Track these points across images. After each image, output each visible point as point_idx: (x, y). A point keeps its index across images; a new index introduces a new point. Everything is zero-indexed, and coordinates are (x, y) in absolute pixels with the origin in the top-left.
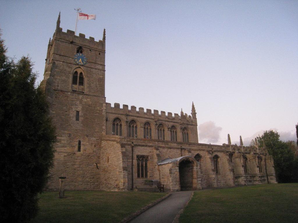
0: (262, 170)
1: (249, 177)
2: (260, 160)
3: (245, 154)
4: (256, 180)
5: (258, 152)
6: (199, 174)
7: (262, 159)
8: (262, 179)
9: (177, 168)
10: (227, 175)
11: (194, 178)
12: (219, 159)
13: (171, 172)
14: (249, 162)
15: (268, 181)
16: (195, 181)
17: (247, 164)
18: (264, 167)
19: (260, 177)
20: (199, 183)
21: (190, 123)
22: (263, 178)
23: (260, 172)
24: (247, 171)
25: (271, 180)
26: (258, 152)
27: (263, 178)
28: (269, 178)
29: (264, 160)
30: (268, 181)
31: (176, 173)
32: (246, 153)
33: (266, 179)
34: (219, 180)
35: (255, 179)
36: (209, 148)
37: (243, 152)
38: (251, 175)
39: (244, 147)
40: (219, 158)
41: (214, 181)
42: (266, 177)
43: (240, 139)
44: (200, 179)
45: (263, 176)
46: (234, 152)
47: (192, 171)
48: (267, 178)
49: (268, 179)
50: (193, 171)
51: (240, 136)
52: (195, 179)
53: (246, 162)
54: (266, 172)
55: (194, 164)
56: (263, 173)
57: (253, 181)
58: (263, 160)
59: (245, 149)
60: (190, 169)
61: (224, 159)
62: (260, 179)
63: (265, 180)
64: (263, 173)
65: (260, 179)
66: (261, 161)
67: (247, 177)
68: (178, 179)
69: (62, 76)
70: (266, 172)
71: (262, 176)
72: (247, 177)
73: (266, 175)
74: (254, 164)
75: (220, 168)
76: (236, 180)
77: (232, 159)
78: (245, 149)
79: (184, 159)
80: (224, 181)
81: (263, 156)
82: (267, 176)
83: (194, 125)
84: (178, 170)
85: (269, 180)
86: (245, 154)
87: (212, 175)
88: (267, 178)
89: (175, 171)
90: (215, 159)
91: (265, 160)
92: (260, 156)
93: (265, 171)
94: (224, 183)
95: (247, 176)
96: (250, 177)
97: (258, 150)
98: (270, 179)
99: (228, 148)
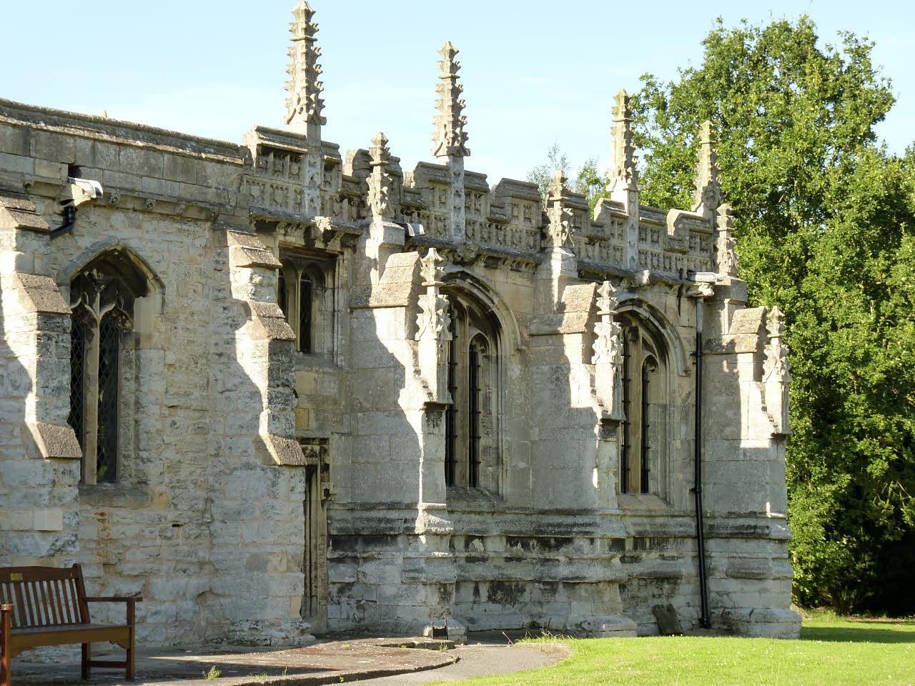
0: (655, 468)
1: (496, 546)
2: (639, 355)
3: (479, 271)
4: (571, 584)
5: (631, 253)
7: (663, 349)
8: (637, 569)
10: (231, 505)
12: (147, 311)
14: (515, 370)
15: (703, 591)
17: (486, 380)
18: (682, 433)
19: (618, 544)
22: (651, 560)
23: (625, 487)
24: (486, 470)
25: (733, 585)
26: (631, 253)
27: (651, 560)
28: (719, 553)
29: (690, 348)
30: (703, 591)
32: (493, 261)
33: (687, 567)
34: (126, 568)
35: (564, 571)
37: (458, 238)
38: (524, 525)
39: (475, 185)
40: (155, 294)
42: (690, 545)
45: (660, 540)
48: (702, 557)
49: (704, 572)
53: (481, 360)
54: (697, 491)
56: (666, 500)
57: (533, 592)
58: (679, 357)
59: (484, 206)
61: (15, 404)
62: (618, 569)
63: (673, 579)
64: (666, 500)
65: (618, 569)
66: (650, 360)
67: (469, 539)
69: (828, 116)
70: (697, 491)
71: (639, 541)
72: (469, 539)
73: (693, 531)
75: (152, 419)
76: (345, 573)
77: (318, 319)
78: (484, 206)
80: (195, 583)
81: (685, 304)
82: (701, 538)
85: (713, 585)
86: (479, 271)
87: (31, 500)
88: (702, 557)
90: (322, 209)
91: (698, 355)
92: (652, 310)
93: (682, 477)
95: (473, 523)
96: (511, 541)
97: (632, 236)
99: (281, 181)
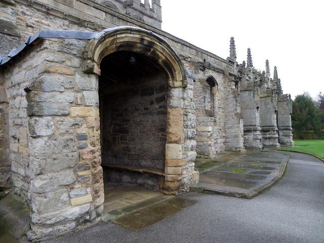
6: (189, 123)
9: (94, 82)
11: (174, 138)
13: (30, 90)
16: (174, 151)
20: (189, 158)
21: (148, 12)
31: (76, 111)
35: (268, 136)
36: (197, 55)
39: (255, 72)
40: (216, 86)
41: (209, 143)
43: (247, 54)
44: (193, 143)
46: (241, 78)
47: (165, 107)
50: (169, 110)
51: (249, 49)
52: (176, 142)
55: (173, 77)
60: (152, 103)
68: (93, 150)
74: (269, 106)
79: (130, 44)
83: (155, 19)
84: (93, 97)
89: (70, 96)
94: (222, 144)
98: (282, 136)
